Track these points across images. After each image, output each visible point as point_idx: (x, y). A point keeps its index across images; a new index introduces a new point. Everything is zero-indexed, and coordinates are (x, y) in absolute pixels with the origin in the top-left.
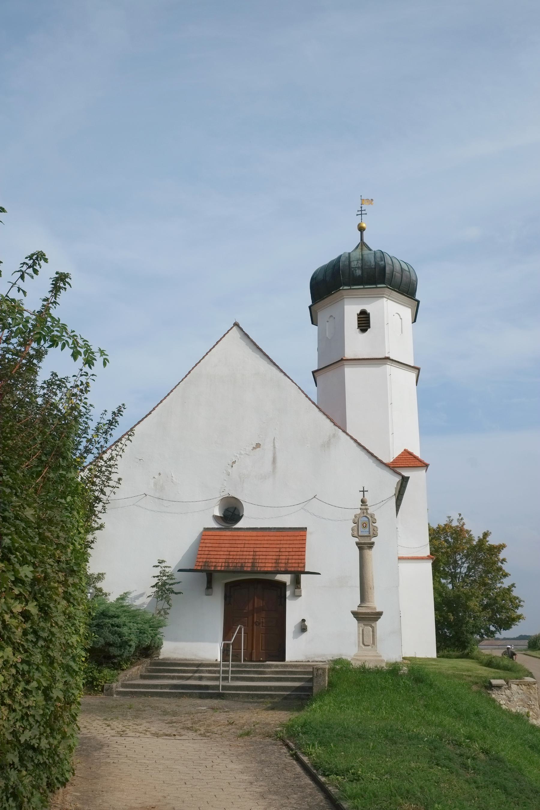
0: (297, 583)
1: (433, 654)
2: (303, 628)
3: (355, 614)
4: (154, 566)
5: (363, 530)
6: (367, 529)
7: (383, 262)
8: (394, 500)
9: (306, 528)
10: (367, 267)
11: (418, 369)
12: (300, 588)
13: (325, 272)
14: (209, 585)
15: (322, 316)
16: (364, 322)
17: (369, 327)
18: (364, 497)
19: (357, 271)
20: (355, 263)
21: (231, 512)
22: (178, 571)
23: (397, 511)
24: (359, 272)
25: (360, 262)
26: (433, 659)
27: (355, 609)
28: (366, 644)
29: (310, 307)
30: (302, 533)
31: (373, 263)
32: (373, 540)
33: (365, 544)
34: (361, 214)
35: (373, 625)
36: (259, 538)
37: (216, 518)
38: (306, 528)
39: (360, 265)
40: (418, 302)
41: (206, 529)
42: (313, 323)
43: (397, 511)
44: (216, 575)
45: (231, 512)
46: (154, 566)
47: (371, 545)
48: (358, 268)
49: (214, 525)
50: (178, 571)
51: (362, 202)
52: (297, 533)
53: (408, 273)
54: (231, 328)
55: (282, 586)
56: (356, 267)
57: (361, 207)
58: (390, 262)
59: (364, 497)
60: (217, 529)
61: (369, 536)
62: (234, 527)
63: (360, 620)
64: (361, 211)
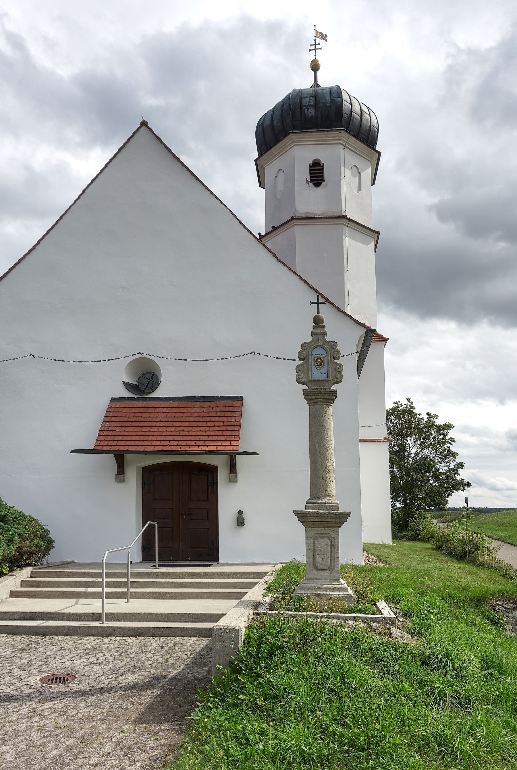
0: (233, 468)
1: (388, 540)
2: (241, 522)
3: (301, 516)
4: (73, 452)
5: (314, 370)
6: (324, 370)
7: (339, 99)
8: (356, 357)
9: (242, 397)
10: (321, 105)
11: (378, 233)
12: (236, 473)
13: (272, 119)
14: (121, 469)
15: (270, 172)
16: (317, 174)
17: (323, 180)
18: (318, 312)
19: (310, 110)
20: (308, 99)
21: (145, 379)
22: (71, 453)
23: (359, 376)
24: (311, 112)
25: (313, 98)
26: (385, 546)
27: (302, 508)
28: (320, 566)
29: (256, 161)
30: (237, 403)
31: (328, 100)
32: (334, 387)
33: (317, 394)
34: (315, 49)
35: (333, 535)
36: (181, 410)
37: (127, 385)
38: (242, 397)
39: (313, 102)
40: (379, 153)
41: (113, 400)
42: (260, 186)
43: (359, 376)
44: (128, 457)
45: (145, 379)
46: (73, 452)
47: (330, 397)
48: (311, 106)
49: (126, 394)
50: (71, 453)
51: (316, 34)
52: (230, 403)
53: (368, 116)
54: (138, 129)
55: (213, 470)
56: (308, 105)
57: (315, 40)
58: (349, 100)
59: (318, 312)
60: (128, 399)
61: (328, 381)
62: (149, 396)
63: (310, 527)
64: (315, 45)
